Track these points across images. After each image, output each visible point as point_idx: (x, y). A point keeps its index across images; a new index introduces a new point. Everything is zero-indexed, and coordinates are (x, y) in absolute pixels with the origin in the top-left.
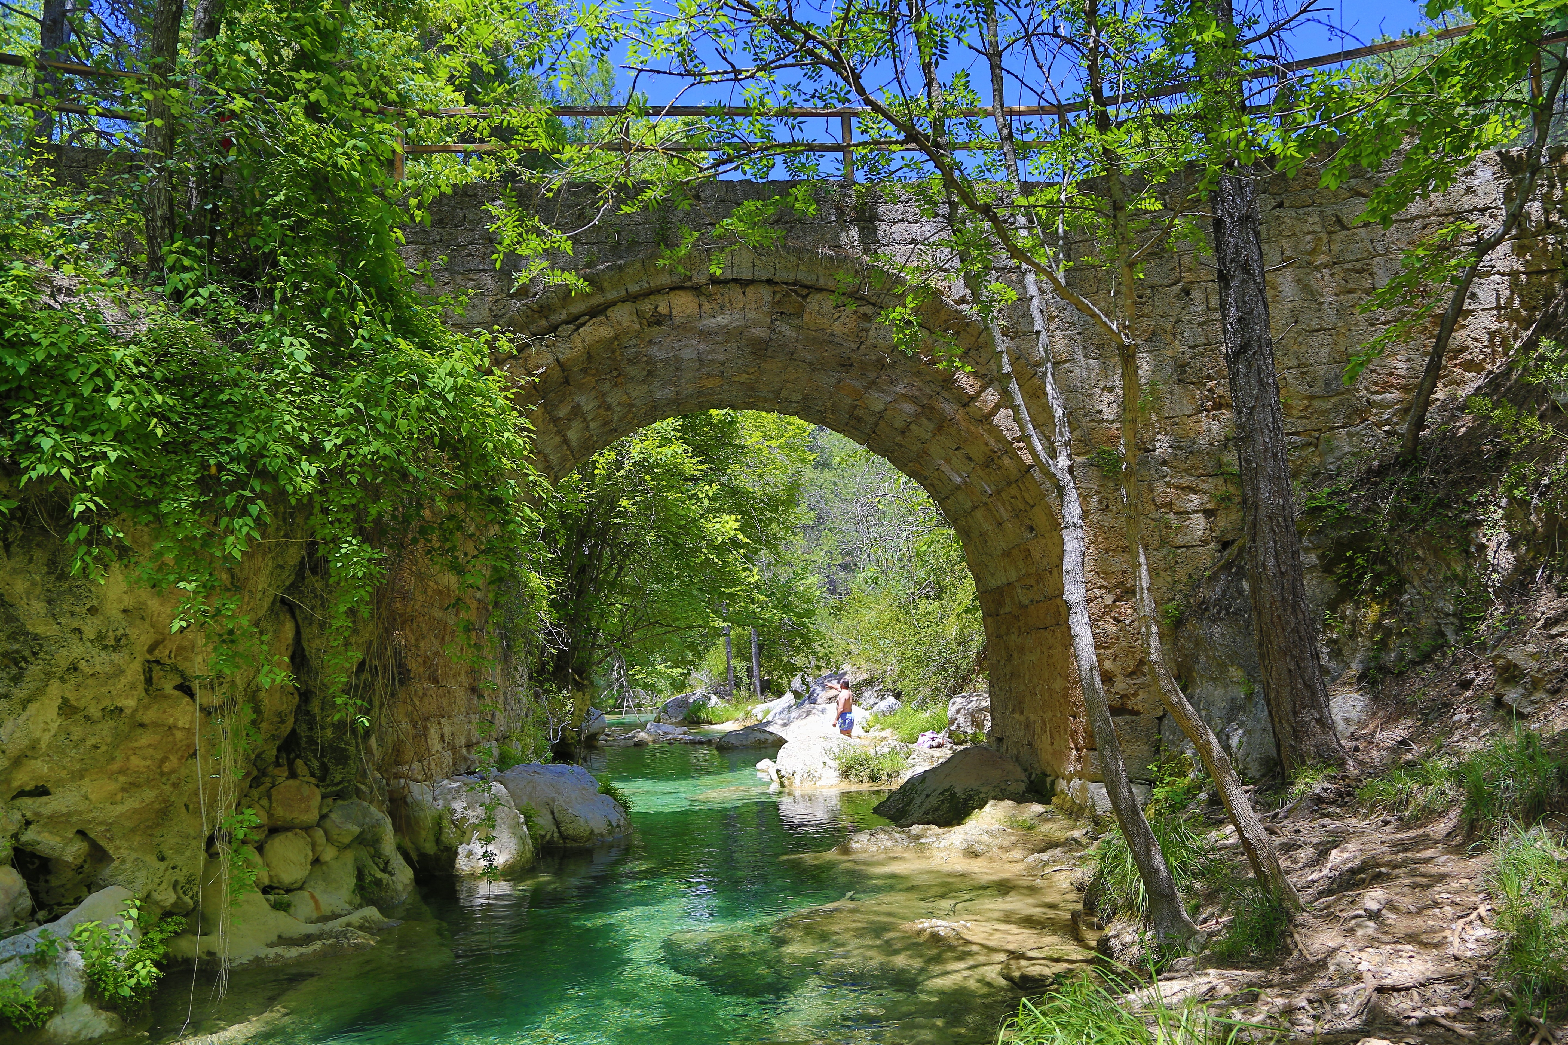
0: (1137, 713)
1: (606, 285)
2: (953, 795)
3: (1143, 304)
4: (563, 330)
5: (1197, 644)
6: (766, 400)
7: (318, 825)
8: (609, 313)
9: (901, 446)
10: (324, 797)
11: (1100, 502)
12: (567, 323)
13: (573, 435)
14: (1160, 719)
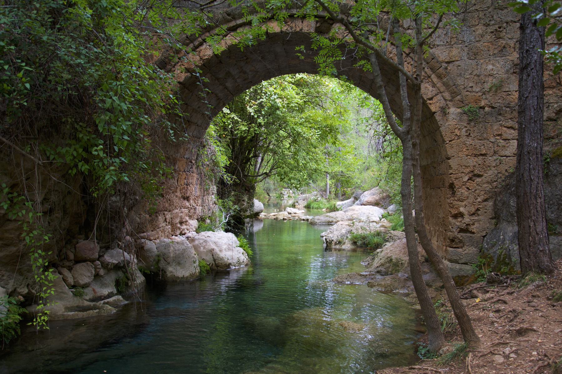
0: (473, 233)
2: (391, 260)
3: (501, 32)
5: (503, 204)
7: (98, 260)
10: (100, 248)
11: (466, 131)
13: (229, 84)
14: (484, 237)
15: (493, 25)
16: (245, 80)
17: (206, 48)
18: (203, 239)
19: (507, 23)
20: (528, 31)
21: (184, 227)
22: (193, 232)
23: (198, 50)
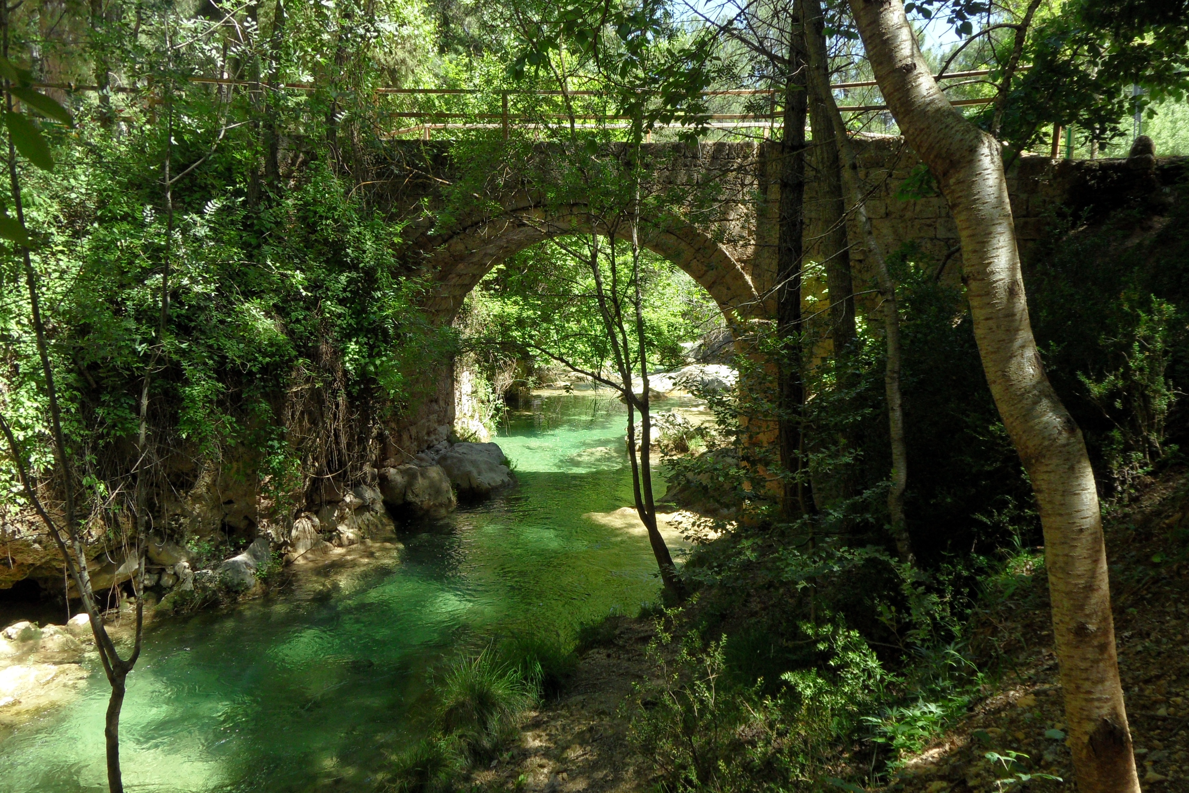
21: (433, 437)
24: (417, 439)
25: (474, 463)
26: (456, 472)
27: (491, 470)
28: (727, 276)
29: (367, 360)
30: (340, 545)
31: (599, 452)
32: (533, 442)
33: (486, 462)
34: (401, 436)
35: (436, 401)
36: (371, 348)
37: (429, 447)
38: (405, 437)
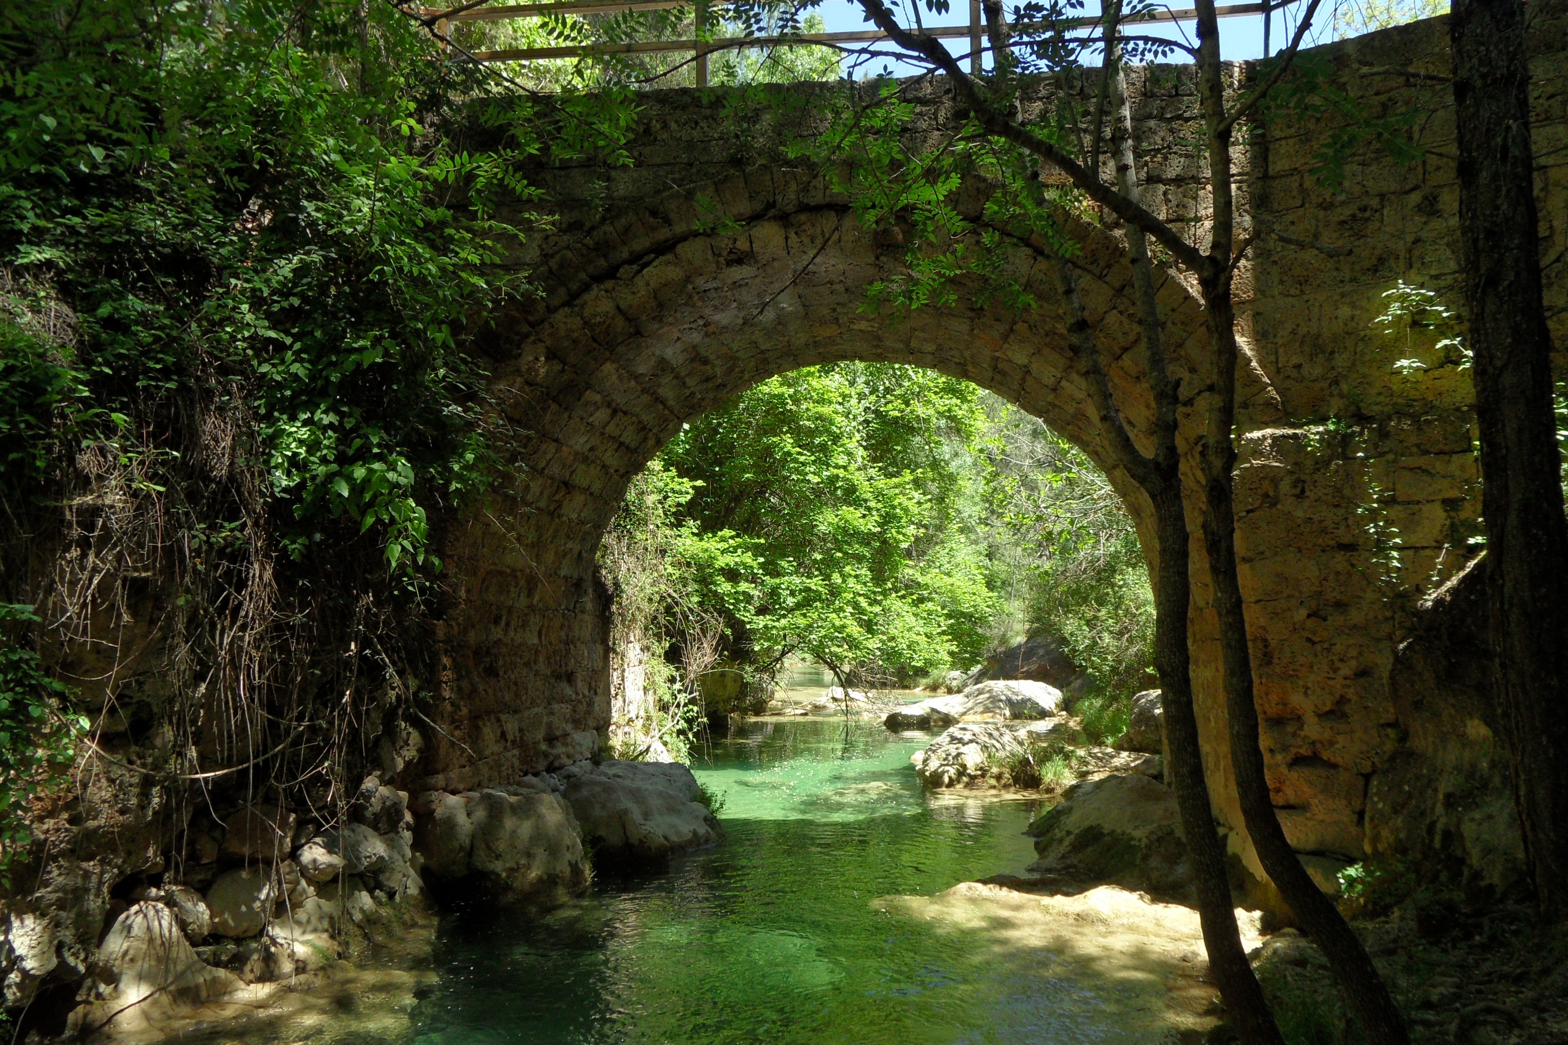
1: (672, 215)
3: (1367, 220)
4: (625, 271)
6: (895, 351)
8: (679, 249)
9: (1054, 406)
12: (630, 262)
15: (1343, 203)
16: (707, 380)
17: (597, 298)
18: (600, 783)
19: (1382, 196)
20: (1484, 176)
21: (560, 749)
22: (584, 763)
23: (577, 302)
24: (520, 743)
25: (636, 794)
26: (597, 812)
27: (672, 810)
28: (1188, 342)
29: (334, 467)
30: (267, 976)
31: (875, 788)
32: (754, 777)
33: (660, 794)
34: (477, 728)
35: (570, 678)
36: (344, 436)
37: (551, 769)
38: (489, 732)
